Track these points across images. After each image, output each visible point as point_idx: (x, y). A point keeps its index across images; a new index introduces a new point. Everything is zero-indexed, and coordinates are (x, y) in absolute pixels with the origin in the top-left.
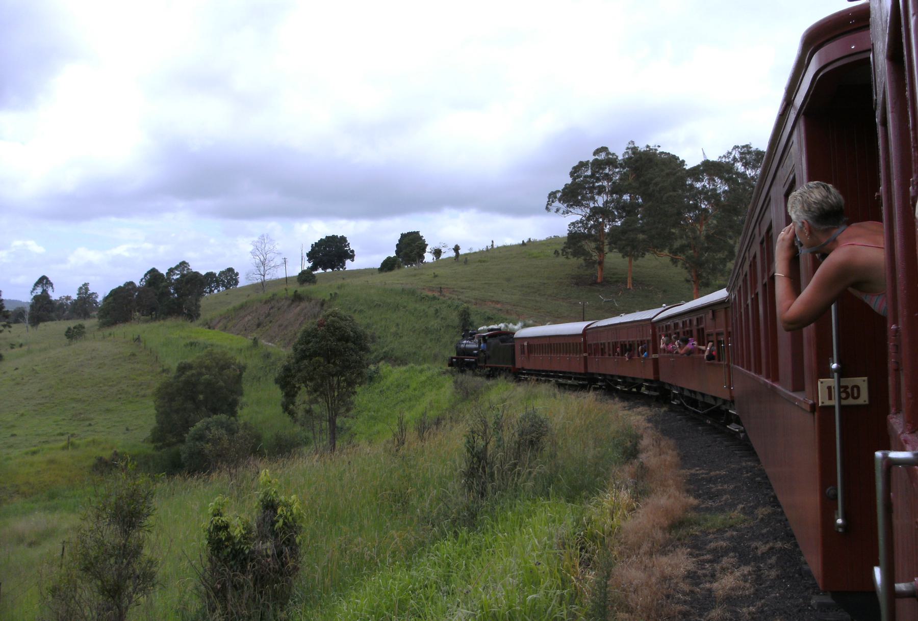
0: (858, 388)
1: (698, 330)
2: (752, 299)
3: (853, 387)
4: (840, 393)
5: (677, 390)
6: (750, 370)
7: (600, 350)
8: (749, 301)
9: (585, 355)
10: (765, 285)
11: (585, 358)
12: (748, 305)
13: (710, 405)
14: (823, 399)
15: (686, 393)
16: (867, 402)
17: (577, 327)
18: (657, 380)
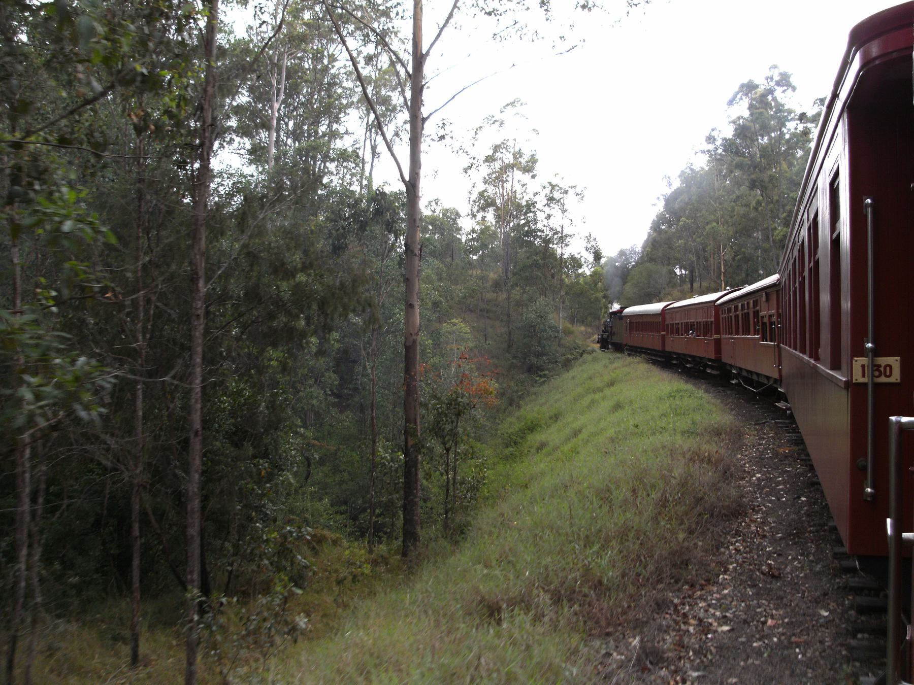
0: (890, 366)
1: (754, 312)
2: (800, 282)
3: (886, 366)
4: (873, 371)
5: (736, 370)
6: (796, 350)
7: (675, 329)
8: (797, 285)
9: (663, 333)
10: (810, 269)
11: (663, 337)
12: (796, 288)
13: (763, 384)
14: (858, 377)
15: (744, 373)
16: (899, 381)
17: (656, 307)
18: (718, 360)
